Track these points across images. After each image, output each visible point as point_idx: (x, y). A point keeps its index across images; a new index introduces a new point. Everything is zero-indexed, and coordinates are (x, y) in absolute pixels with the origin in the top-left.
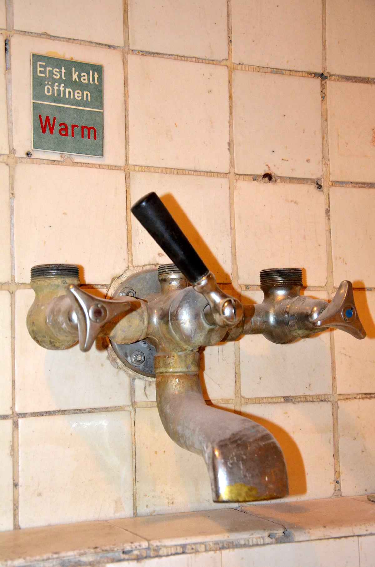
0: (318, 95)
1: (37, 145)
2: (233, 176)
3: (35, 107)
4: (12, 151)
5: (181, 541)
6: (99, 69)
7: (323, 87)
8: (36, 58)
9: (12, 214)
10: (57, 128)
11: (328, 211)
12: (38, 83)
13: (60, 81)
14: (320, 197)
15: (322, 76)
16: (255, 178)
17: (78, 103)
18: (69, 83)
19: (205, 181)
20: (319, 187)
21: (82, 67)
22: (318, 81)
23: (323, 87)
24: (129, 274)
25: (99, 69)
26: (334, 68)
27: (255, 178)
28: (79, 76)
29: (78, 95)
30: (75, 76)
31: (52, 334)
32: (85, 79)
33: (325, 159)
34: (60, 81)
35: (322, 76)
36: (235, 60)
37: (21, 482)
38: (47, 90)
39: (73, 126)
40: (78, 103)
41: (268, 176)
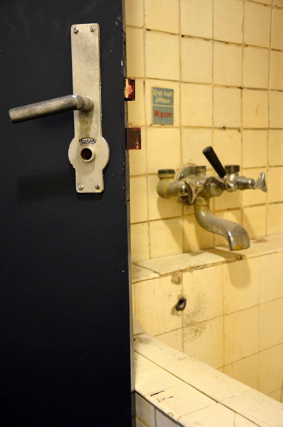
0: (240, 96)
1: (155, 122)
2: (213, 128)
3: (154, 107)
4: (146, 124)
5: (213, 262)
6: (172, 91)
7: (241, 92)
8: (154, 88)
9: (205, 39)
10: (160, 114)
11: (242, 140)
12: (154, 97)
13: (161, 96)
14: (240, 134)
15: (241, 88)
16: (220, 129)
17: (166, 104)
19: (204, 130)
20: (240, 131)
21: (168, 90)
22: (240, 90)
23: (241, 92)
24: (182, 168)
25: (172, 91)
26: (245, 85)
27: (220, 129)
28: (167, 94)
30: (165, 94)
31: (179, 172)
32: (168, 95)
33: (242, 120)
34: (161, 96)
35: (241, 88)
36: (214, 83)
37: (151, 243)
38: (157, 100)
39: (165, 113)
40: (166, 104)
41: (224, 128)
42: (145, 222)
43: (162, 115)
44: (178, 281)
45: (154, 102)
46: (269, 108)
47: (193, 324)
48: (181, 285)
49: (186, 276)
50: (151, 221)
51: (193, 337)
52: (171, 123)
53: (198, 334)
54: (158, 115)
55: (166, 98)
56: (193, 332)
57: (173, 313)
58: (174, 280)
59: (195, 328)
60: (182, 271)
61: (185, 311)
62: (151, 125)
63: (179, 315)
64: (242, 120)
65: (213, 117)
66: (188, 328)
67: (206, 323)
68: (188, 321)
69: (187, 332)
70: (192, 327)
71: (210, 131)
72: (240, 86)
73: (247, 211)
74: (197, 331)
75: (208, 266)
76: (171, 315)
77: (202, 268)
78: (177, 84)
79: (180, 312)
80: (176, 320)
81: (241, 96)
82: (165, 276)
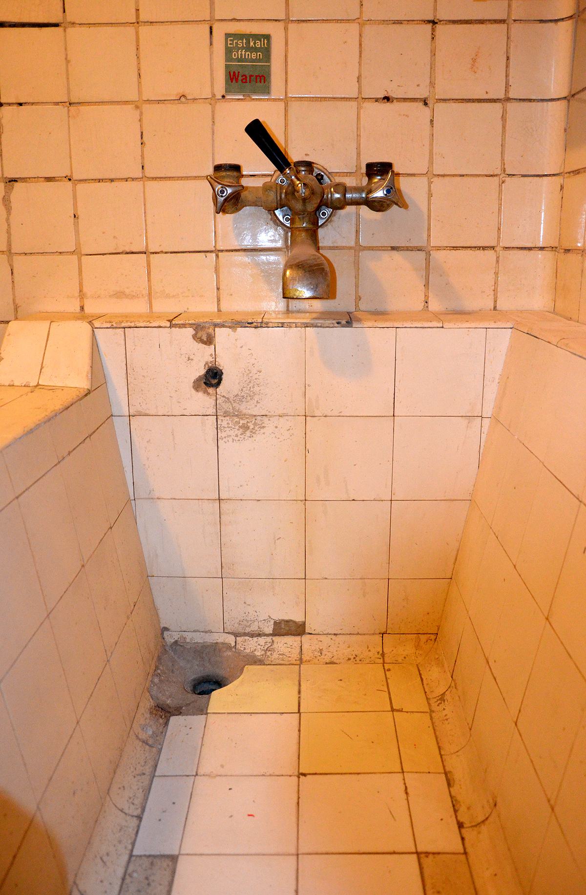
0: (429, 36)
1: (228, 90)
4: (214, 95)
6: (268, 37)
8: (227, 35)
12: (228, 51)
13: (243, 48)
14: (427, 111)
15: (434, 22)
18: (248, 49)
20: (426, 104)
21: (257, 37)
22: (430, 26)
25: (268, 37)
26: (442, 15)
28: (255, 43)
29: (254, 56)
30: (252, 44)
33: (432, 84)
34: (243, 48)
39: (251, 76)
41: (387, 99)
42: (211, 252)
43: (246, 78)
44: (209, 341)
45: (228, 57)
46: (508, 58)
47: (240, 415)
48: (213, 346)
49: (221, 335)
50: (222, 251)
51: (237, 436)
52: (267, 90)
53: (248, 433)
54: (237, 81)
55: (255, 50)
56: (237, 427)
57: (196, 386)
58: (199, 335)
59: (242, 422)
60: (216, 325)
61: (220, 389)
62: (223, 96)
63: (209, 394)
64: (432, 84)
65: (359, 79)
66: (228, 418)
67: (265, 419)
68: (227, 407)
69: (224, 424)
70: (236, 419)
71: (354, 104)
72: (431, 18)
73: (438, 256)
74: (245, 428)
75: (271, 325)
76: (193, 391)
77: (256, 327)
78: (281, 25)
79: (211, 390)
80: (203, 401)
81: (211, 44)
82: (180, 327)
